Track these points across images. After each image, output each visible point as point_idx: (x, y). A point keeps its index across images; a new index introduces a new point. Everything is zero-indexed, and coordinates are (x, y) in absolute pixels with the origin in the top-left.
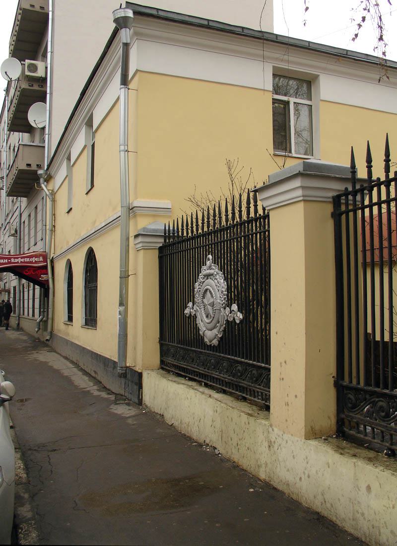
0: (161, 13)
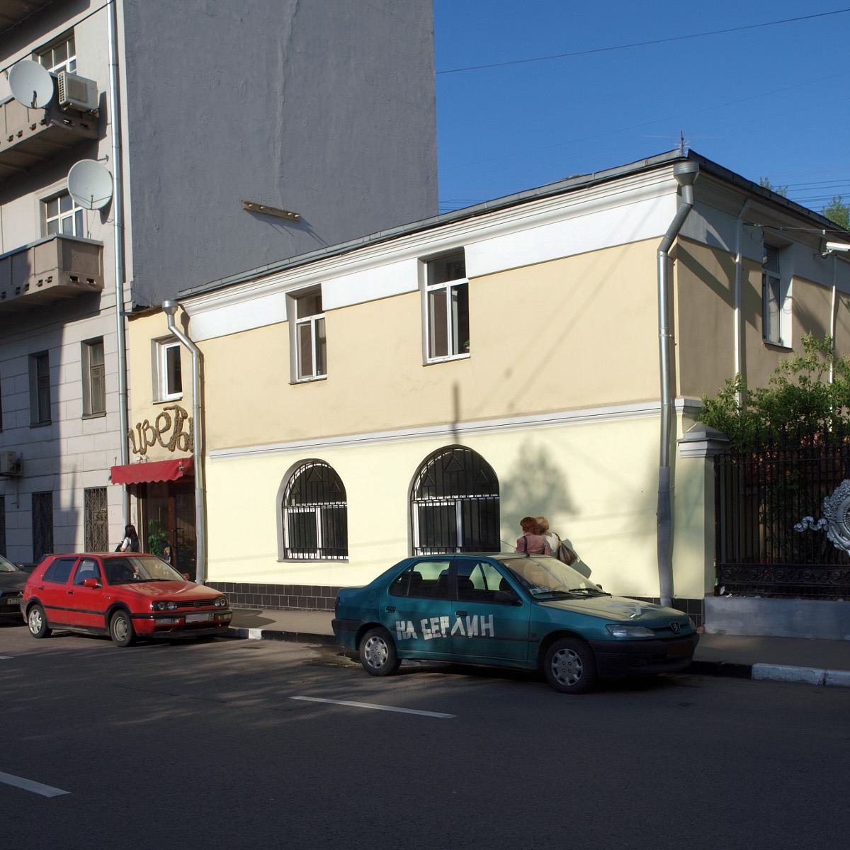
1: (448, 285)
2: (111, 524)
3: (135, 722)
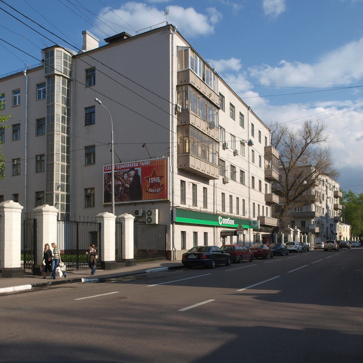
0: (8, 75)
2: (257, 137)
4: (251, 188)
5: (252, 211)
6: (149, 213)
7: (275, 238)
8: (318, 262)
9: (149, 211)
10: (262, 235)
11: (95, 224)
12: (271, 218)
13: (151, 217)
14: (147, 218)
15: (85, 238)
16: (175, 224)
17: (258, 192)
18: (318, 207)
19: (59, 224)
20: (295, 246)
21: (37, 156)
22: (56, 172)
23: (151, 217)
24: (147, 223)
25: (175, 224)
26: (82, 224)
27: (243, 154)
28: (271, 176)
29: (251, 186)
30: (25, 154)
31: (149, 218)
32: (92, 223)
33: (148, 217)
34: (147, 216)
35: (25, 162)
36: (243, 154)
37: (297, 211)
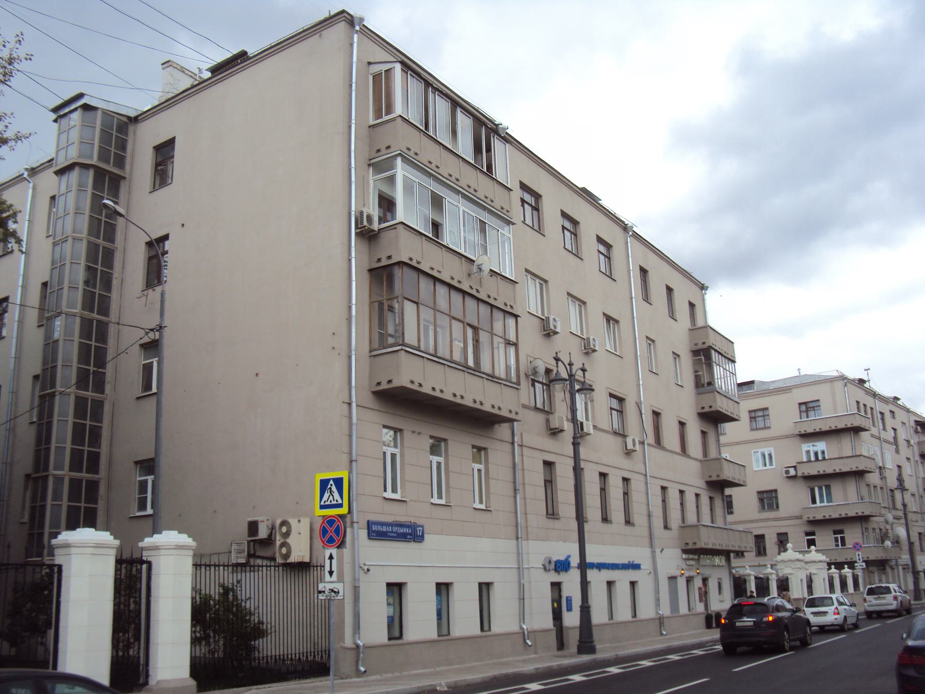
1: (839, 536)
3: (90, 475)
4: (649, 445)
5: (657, 512)
6: (284, 529)
7: (748, 583)
8: (828, 643)
9: (284, 523)
10: (820, 503)
11: (315, 568)
12: (329, 531)
13: (289, 540)
14: (278, 543)
15: (293, 615)
16: (735, 558)
17: (678, 457)
18: (875, 487)
19: (198, 572)
20: (833, 608)
21: (571, 597)
22: (59, 416)
23: (289, 540)
24: (280, 560)
25: (735, 558)
26: (224, 569)
27: (616, 351)
28: (713, 409)
29: (651, 439)
30: (632, 260)
31: (284, 544)
32: (228, 566)
33: (282, 541)
34: (278, 538)
35: (99, 371)
36: (616, 351)
37: (818, 504)
